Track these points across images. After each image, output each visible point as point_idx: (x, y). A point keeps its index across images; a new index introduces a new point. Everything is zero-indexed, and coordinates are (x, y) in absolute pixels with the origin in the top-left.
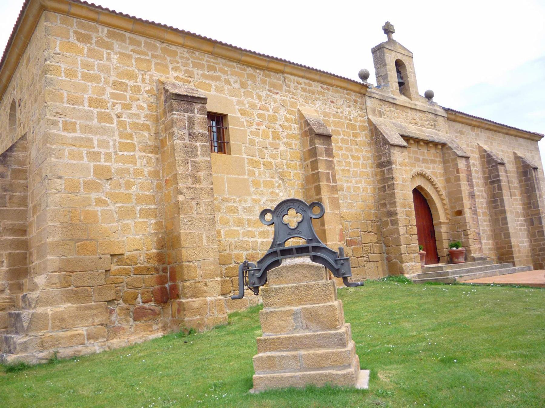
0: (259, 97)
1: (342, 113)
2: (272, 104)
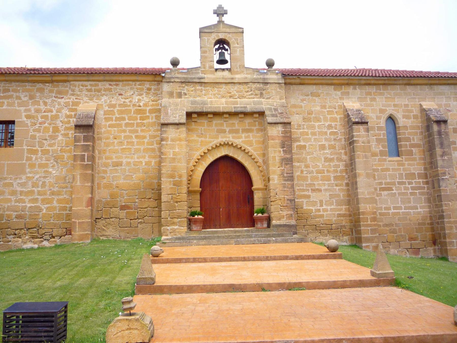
0: (45, 104)
1: (130, 101)
2: (57, 106)
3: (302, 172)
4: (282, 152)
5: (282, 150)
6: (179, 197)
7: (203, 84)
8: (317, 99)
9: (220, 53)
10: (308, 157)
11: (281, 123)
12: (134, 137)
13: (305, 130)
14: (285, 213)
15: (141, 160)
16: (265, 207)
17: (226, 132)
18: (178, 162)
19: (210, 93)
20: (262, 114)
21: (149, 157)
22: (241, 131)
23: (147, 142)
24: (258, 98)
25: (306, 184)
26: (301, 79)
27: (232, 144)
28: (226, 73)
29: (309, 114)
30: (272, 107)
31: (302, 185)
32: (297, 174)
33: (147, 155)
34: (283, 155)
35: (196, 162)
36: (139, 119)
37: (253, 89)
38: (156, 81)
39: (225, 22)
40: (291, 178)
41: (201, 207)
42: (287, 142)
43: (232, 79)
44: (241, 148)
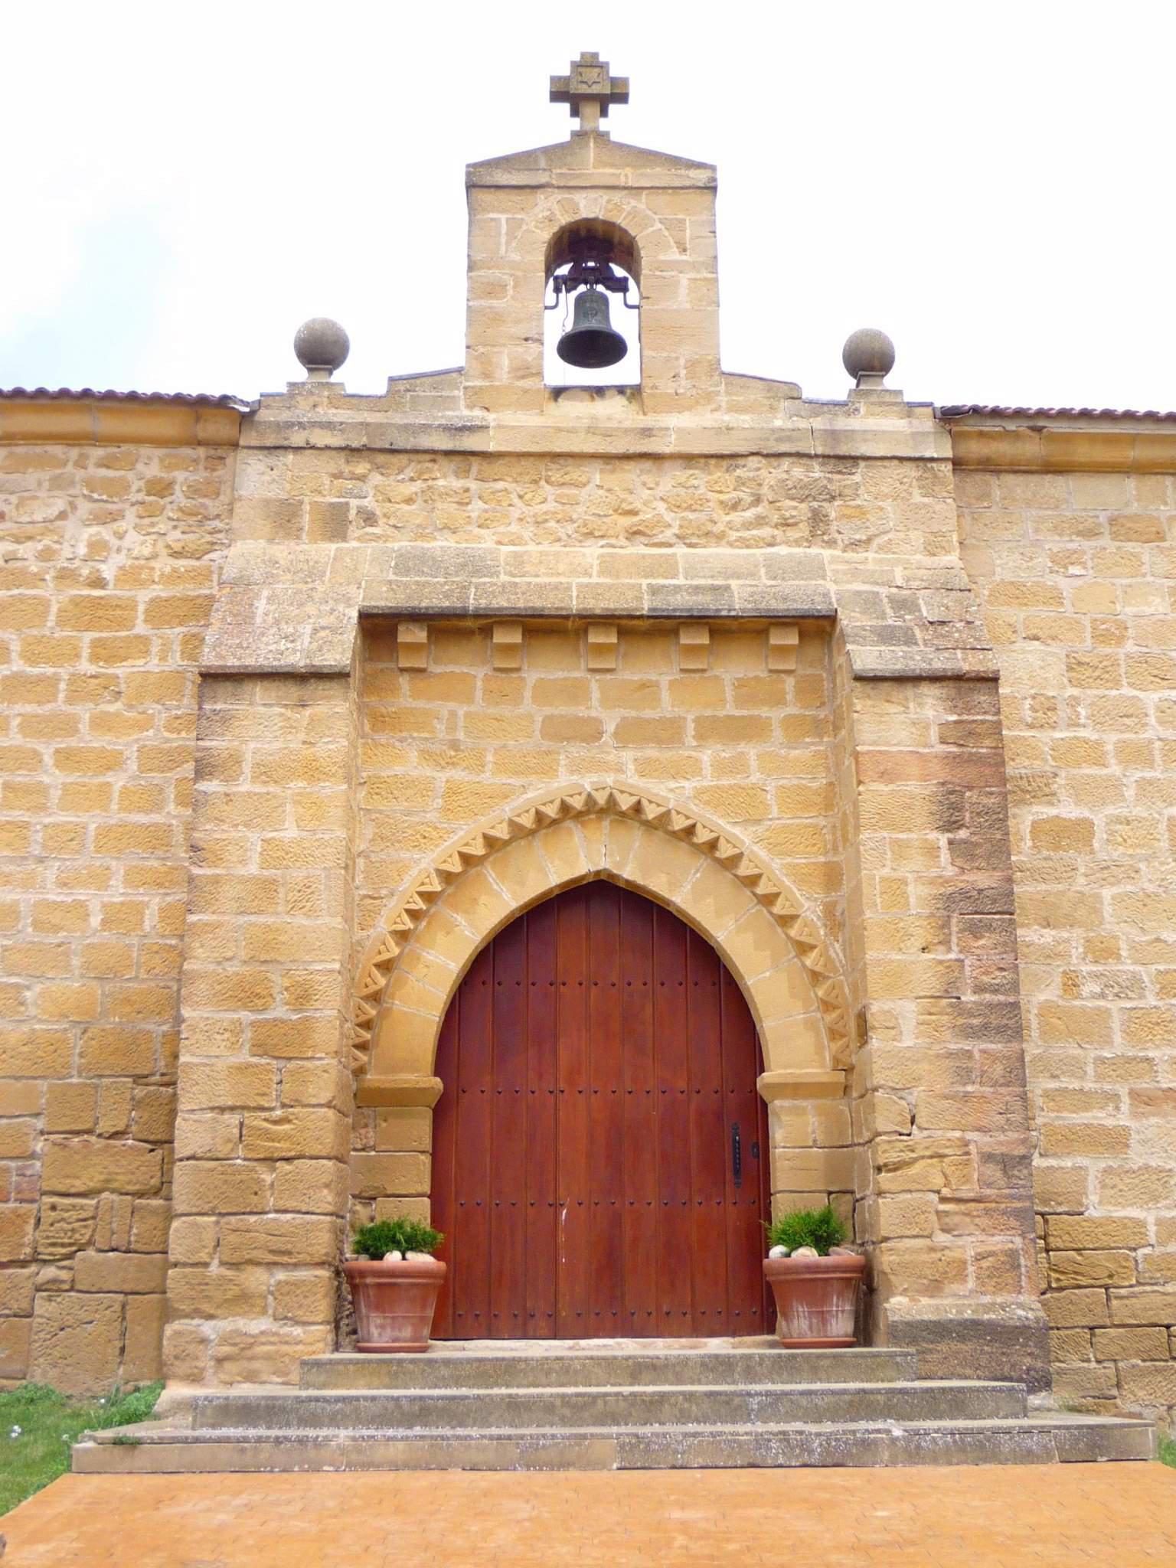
1: (46, 555)
3: (1071, 984)
4: (945, 856)
5: (943, 839)
6: (283, 1133)
7: (476, 465)
8: (1145, 552)
9: (579, 300)
10: (1107, 893)
11: (935, 679)
12: (48, 760)
13: (1083, 733)
14: (969, 1245)
15: (81, 894)
16: (843, 1206)
17: (601, 733)
18: (293, 907)
19: (515, 513)
20: (818, 628)
21: (128, 881)
22: (691, 727)
23: (125, 792)
24: (797, 543)
25: (1101, 1060)
26: (1053, 438)
27: (638, 808)
28: (614, 409)
29: (1101, 637)
30: (884, 591)
31: (1075, 1067)
32: (1042, 997)
33: (118, 868)
34: (950, 871)
35: (414, 915)
36: (86, 652)
37: (765, 490)
38: (200, 443)
39: (614, 137)
40: (1004, 1019)
41: (436, 1196)
42: (977, 796)
43: (647, 432)
44: (690, 831)
